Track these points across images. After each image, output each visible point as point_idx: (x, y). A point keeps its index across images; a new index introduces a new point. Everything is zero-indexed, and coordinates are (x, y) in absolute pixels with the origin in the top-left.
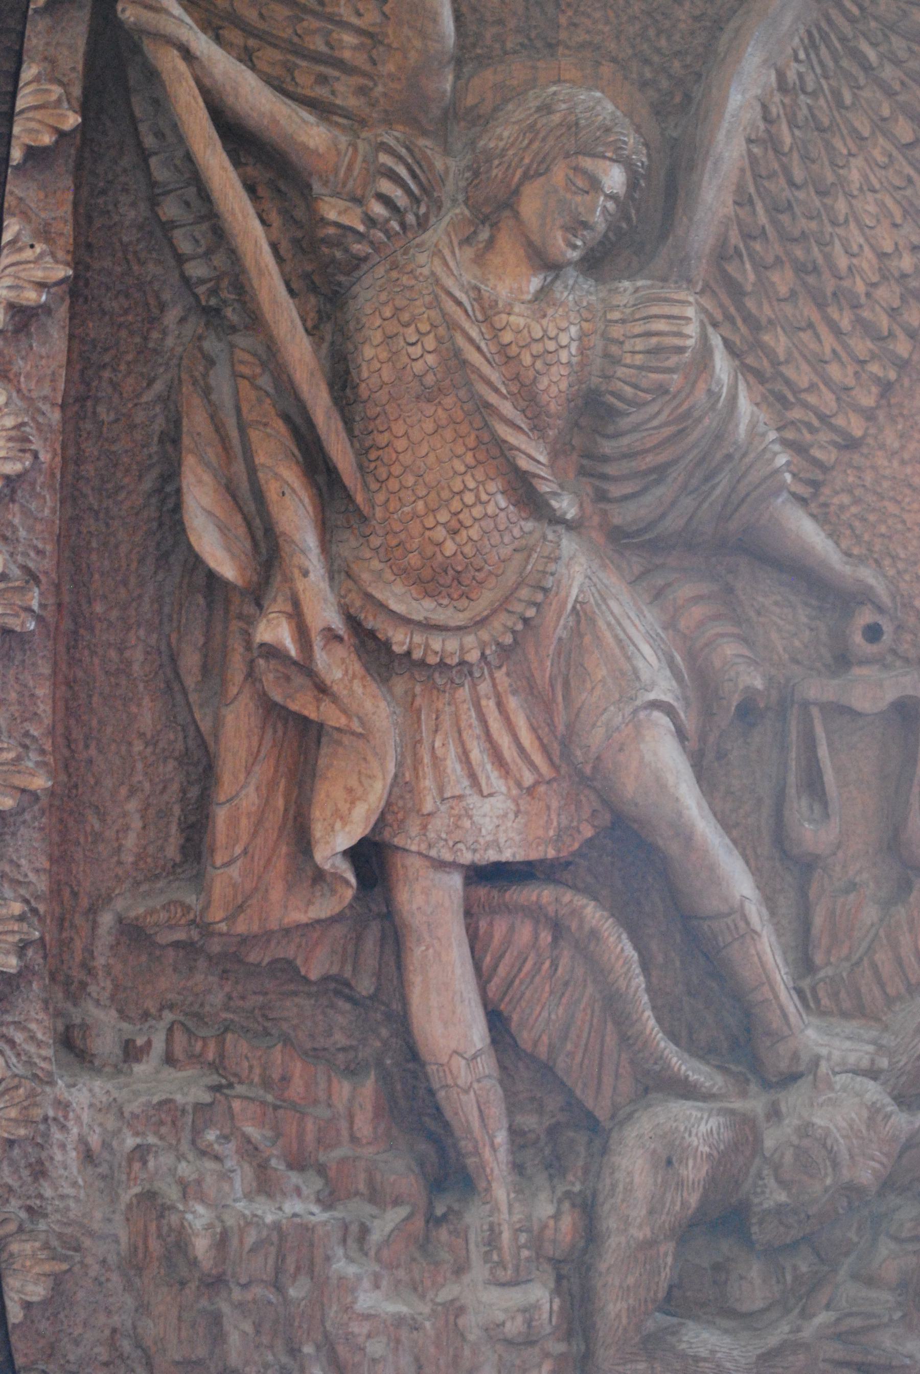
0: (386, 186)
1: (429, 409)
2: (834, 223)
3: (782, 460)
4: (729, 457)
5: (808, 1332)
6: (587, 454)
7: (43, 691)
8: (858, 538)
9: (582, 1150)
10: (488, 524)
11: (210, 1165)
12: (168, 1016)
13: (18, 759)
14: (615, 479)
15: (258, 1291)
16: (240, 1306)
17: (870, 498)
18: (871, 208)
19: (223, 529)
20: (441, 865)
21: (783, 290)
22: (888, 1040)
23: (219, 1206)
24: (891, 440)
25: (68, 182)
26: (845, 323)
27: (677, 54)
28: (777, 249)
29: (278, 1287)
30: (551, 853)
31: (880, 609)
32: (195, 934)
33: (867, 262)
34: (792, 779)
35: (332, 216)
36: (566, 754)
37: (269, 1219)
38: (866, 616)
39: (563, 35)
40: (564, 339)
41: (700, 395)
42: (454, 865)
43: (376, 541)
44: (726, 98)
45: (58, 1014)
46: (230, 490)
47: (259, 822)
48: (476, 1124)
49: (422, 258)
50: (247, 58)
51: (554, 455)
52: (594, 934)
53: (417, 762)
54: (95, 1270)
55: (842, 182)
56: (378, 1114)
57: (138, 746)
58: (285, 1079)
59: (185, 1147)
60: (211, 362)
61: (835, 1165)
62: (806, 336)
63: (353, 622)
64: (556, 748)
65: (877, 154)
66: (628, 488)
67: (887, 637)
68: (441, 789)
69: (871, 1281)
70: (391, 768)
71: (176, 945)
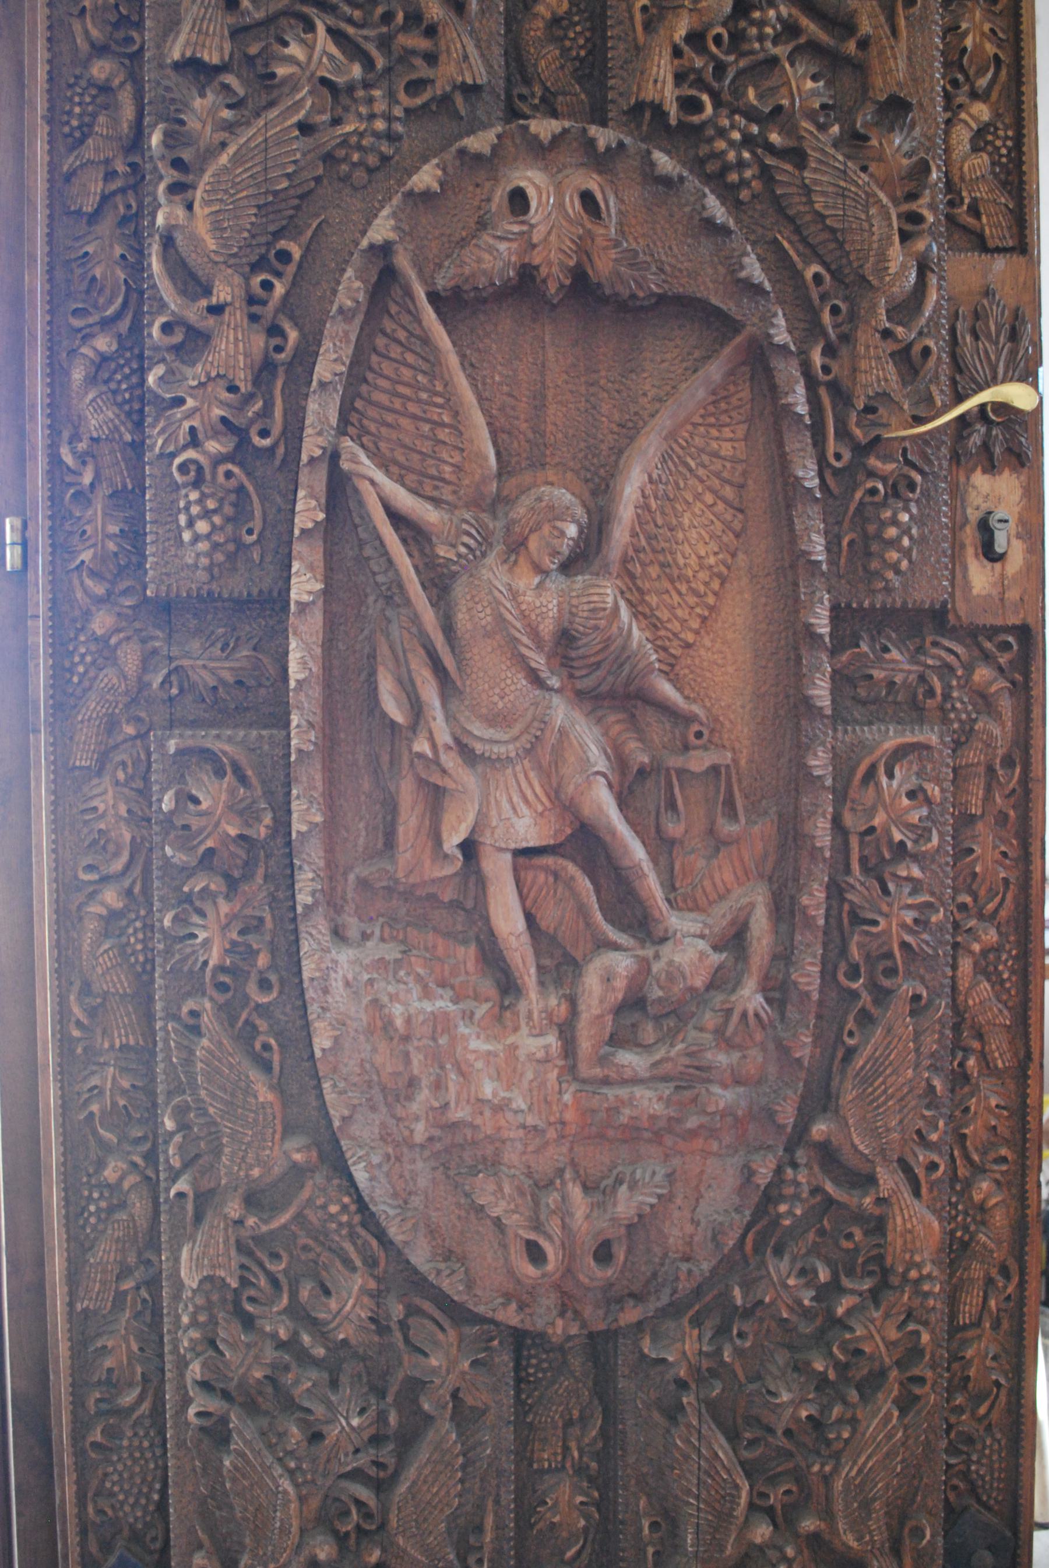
0: (466, 539)
1: (489, 641)
2: (677, 543)
3: (654, 657)
4: (629, 657)
5: (672, 1054)
6: (565, 657)
7: (318, 777)
8: (693, 689)
9: (570, 975)
10: (518, 693)
11: (402, 986)
12: (381, 920)
13: (308, 809)
14: (578, 668)
15: (425, 1041)
16: (418, 1048)
17: (698, 671)
18: (695, 536)
19: (396, 699)
20: (501, 850)
21: (654, 575)
22: (710, 921)
23: (406, 1004)
24: (707, 642)
25: (321, 543)
26: (684, 590)
27: (602, 466)
28: (651, 556)
29: (434, 1039)
30: (552, 842)
31: (701, 724)
32: (391, 883)
33: (693, 561)
34: (663, 804)
35: (442, 554)
36: (557, 797)
37: (429, 1010)
38: (696, 727)
39: (548, 460)
40: (550, 606)
41: (614, 629)
42: (507, 849)
43: (467, 703)
44: (623, 490)
45: (332, 920)
46: (400, 681)
47: (419, 832)
48: (521, 965)
49: (484, 571)
50: (401, 480)
51: (549, 658)
52: (572, 878)
53: (488, 803)
54: (352, 1033)
55: (681, 524)
56: (477, 961)
57: (363, 798)
58: (435, 947)
59: (391, 978)
60: (389, 621)
61: (684, 978)
62: (666, 597)
63: (457, 740)
64: (553, 795)
65: (697, 510)
66: (583, 672)
67: (706, 737)
68: (500, 815)
69: (701, 1029)
70: (477, 807)
71: (384, 888)
